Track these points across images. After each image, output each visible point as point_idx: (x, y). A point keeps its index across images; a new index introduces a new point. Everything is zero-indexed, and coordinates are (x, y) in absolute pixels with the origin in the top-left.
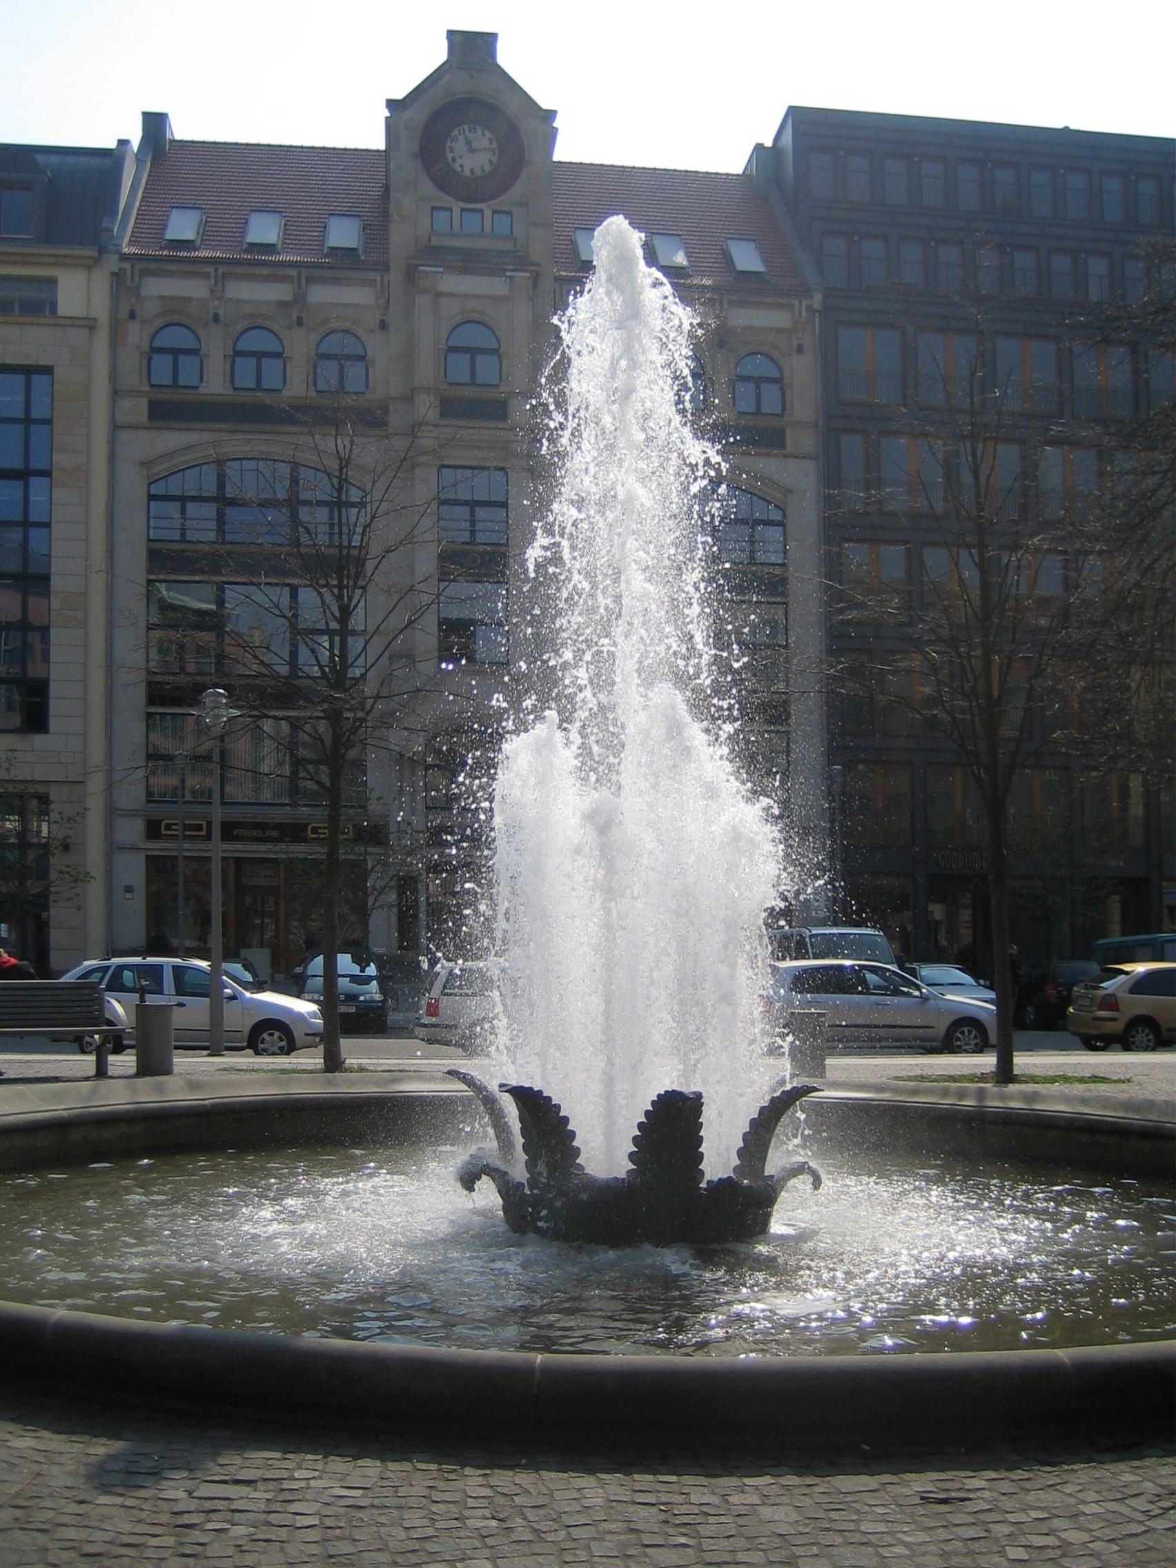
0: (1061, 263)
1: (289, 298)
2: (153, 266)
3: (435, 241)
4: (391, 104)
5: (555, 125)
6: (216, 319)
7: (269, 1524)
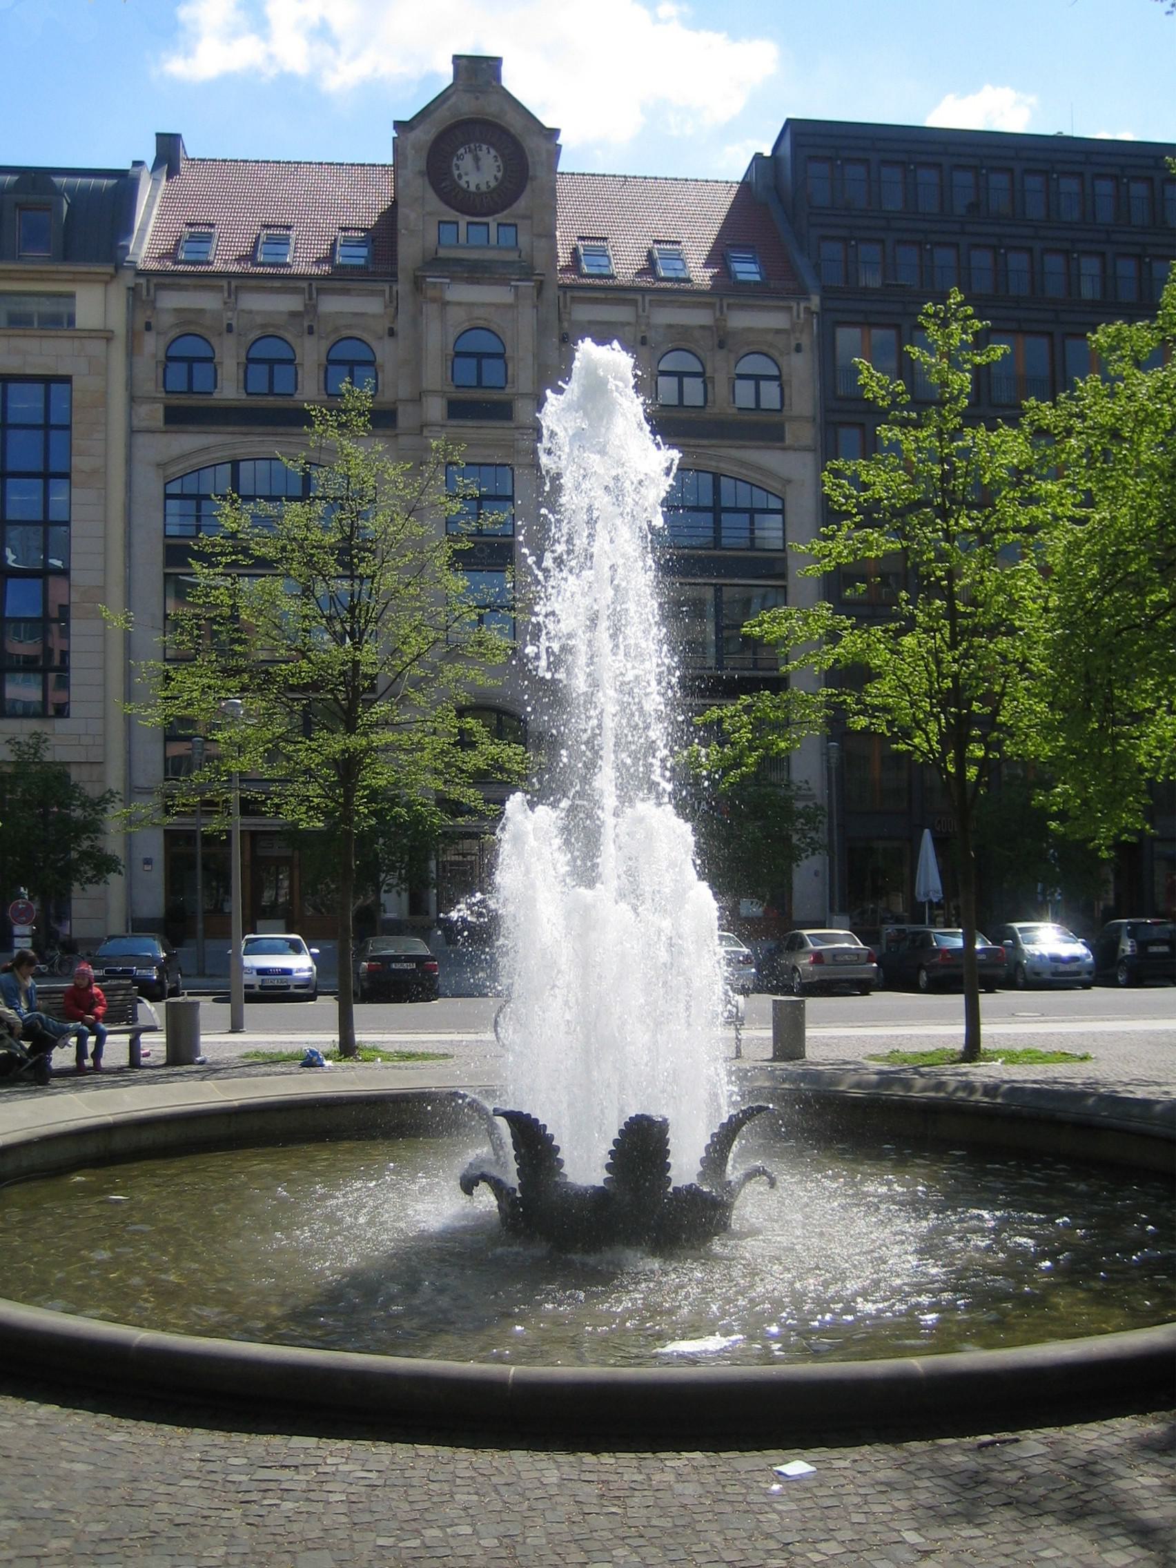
0: (1054, 263)
1: (300, 308)
2: (167, 281)
3: (443, 253)
4: (398, 125)
5: (558, 142)
6: (230, 328)
7: (308, 1499)
